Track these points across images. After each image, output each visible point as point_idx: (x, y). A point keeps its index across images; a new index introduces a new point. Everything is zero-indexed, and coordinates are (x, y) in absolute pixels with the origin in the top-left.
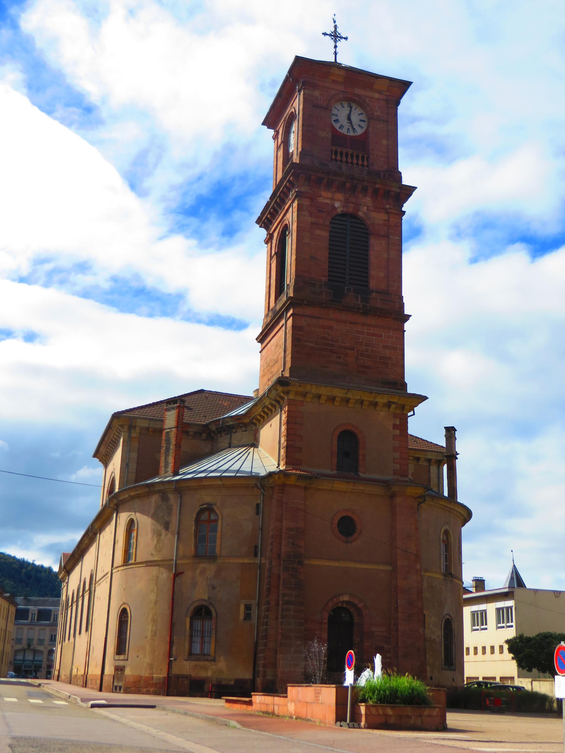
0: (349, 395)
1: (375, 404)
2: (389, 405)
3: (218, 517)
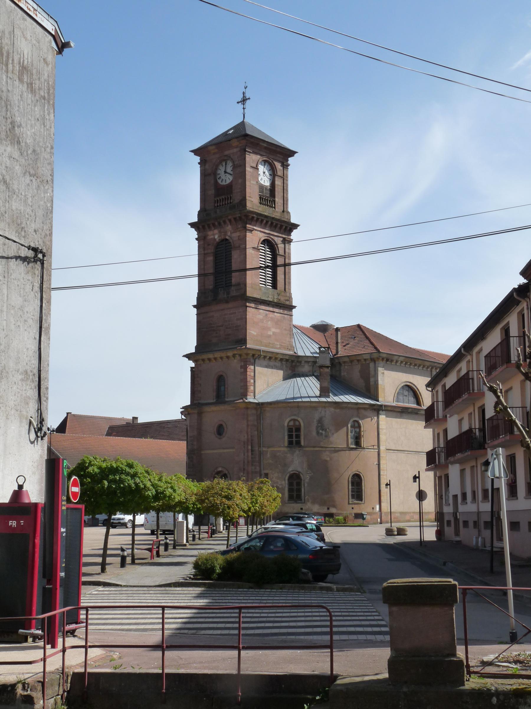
0: (216, 356)
1: (228, 357)
2: (234, 356)
3: (299, 422)
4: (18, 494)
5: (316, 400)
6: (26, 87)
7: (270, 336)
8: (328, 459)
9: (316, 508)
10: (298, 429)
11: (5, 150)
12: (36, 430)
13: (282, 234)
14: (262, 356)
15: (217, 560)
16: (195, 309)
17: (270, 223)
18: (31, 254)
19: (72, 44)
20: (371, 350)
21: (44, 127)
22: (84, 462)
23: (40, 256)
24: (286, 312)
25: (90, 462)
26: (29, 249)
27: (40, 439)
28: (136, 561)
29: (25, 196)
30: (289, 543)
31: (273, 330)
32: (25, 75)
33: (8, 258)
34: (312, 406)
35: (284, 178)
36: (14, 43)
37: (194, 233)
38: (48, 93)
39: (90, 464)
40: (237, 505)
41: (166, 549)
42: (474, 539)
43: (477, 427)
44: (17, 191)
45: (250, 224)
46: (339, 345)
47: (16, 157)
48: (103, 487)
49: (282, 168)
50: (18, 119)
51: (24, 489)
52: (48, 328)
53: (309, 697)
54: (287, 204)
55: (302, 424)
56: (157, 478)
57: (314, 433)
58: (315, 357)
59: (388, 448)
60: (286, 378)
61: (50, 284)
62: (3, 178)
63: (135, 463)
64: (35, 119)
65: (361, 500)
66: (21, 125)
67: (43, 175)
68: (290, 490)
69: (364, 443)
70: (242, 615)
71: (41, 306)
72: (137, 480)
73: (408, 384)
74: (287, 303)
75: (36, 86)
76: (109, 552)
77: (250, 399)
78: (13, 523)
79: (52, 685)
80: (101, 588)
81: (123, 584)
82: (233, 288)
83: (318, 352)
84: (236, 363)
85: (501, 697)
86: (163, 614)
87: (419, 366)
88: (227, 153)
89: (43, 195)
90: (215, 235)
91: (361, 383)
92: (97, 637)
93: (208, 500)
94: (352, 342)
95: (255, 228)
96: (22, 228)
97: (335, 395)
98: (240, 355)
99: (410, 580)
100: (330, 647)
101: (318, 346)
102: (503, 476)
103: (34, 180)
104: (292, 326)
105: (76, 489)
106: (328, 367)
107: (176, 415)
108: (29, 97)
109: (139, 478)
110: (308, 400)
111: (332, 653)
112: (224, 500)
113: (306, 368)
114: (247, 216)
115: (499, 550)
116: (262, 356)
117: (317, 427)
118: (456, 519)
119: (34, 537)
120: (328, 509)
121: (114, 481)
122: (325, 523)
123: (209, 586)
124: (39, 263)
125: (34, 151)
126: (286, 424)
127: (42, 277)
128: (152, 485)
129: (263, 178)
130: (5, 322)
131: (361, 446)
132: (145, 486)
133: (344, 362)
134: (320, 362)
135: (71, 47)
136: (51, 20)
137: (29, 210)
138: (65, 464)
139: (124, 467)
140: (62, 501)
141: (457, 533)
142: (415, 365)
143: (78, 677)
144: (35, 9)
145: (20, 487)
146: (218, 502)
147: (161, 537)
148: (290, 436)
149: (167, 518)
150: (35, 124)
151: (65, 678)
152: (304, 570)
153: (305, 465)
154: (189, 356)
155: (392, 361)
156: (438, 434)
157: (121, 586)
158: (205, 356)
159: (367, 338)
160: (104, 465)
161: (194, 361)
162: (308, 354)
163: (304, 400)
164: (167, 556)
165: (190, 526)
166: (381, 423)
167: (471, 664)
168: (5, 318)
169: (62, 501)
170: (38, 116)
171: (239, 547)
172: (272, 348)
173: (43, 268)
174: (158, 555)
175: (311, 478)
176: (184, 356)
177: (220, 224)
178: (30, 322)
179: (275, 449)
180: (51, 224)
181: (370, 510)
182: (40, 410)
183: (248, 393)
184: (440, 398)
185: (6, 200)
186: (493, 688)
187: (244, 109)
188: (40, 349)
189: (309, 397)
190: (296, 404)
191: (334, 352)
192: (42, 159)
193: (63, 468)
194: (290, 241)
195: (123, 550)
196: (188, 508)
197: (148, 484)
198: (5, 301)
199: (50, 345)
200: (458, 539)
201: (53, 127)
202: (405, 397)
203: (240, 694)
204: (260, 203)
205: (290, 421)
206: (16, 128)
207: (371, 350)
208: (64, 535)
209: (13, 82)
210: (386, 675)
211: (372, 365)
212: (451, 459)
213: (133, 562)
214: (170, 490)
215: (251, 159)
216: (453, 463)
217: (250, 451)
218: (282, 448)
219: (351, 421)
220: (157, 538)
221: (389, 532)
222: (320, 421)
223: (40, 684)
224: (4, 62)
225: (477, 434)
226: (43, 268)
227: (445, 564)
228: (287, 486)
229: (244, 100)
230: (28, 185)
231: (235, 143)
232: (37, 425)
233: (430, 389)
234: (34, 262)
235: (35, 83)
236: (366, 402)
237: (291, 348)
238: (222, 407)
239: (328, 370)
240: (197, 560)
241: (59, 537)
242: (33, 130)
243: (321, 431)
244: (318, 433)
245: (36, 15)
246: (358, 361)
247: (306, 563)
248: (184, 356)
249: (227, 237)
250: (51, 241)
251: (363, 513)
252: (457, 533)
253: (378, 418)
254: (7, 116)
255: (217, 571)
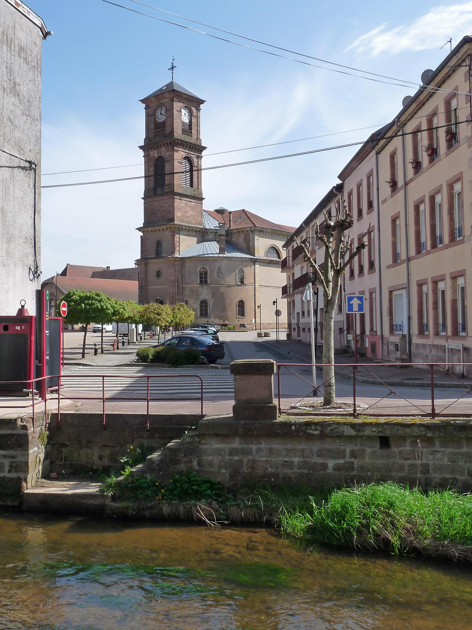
0: (156, 229)
1: (163, 230)
2: (167, 229)
4: (21, 311)
5: (217, 255)
6: (23, 60)
7: (189, 217)
8: (224, 291)
9: (216, 321)
10: (206, 273)
11: (10, 100)
12: (34, 273)
13: (196, 153)
14: (184, 229)
15: (150, 351)
16: (143, 200)
17: (188, 146)
18: (27, 165)
19: (52, 33)
20: (250, 225)
21: (35, 85)
22: (70, 293)
23: (33, 166)
24: (198, 202)
25: (74, 293)
26: (26, 162)
27: (36, 278)
28: (104, 352)
29: (23, 128)
30: (194, 341)
31: (191, 213)
32: (22, 53)
33: (13, 167)
34: (214, 260)
35: (198, 118)
36: (15, 33)
37: (142, 153)
38: (37, 64)
39: (74, 294)
40: (164, 319)
41: (123, 345)
42: (308, 339)
43: (311, 272)
44: (18, 125)
45: (176, 147)
46: (231, 222)
47: (17, 104)
48: (82, 308)
49: (196, 111)
50: (18, 80)
51: (25, 308)
52: (40, 211)
53: (189, 427)
54: (199, 134)
55: (208, 271)
56: (114, 303)
57: (216, 276)
58: (217, 229)
59: (260, 285)
60: (198, 243)
61: (40, 184)
62: (9, 118)
63: (101, 293)
64: (29, 80)
65: (244, 316)
66: (20, 84)
67: (34, 115)
68: (201, 310)
69: (246, 282)
70: (149, 380)
71: (35, 197)
72: (102, 304)
73: (273, 246)
74: (199, 196)
75: (29, 59)
76: (86, 347)
77: (177, 255)
78: (18, 328)
79: (39, 420)
80: (81, 367)
81: (94, 365)
82: (166, 187)
83: (218, 226)
84: (168, 234)
85: (297, 426)
86: (103, 379)
87: (280, 234)
88: (162, 102)
89: (34, 128)
90: (155, 154)
91: (244, 245)
92: (73, 394)
93: (147, 315)
94: (239, 220)
95: (179, 149)
96: (22, 149)
97: (229, 253)
98: (170, 228)
99: (247, 360)
100: (201, 399)
101: (218, 223)
102: (312, 300)
103: (29, 119)
104: (202, 211)
105: (65, 309)
106: (224, 235)
107: (133, 266)
108: (24, 66)
109: (103, 302)
110: (212, 255)
111: (202, 403)
112: (156, 315)
113: (211, 236)
114: (174, 142)
115: (321, 345)
116: (184, 229)
117: (218, 272)
118: (299, 327)
119: (31, 336)
120: (224, 321)
121: (88, 304)
122: (222, 329)
123: (145, 366)
124: (32, 170)
125: (28, 100)
126: (198, 270)
127: (35, 179)
128: (111, 307)
129: (184, 117)
130: (12, 207)
131: (244, 284)
132: (107, 307)
133: (234, 233)
134: (219, 233)
135: (51, 34)
136: (38, 18)
137: (26, 137)
138: (47, 293)
139: (94, 296)
140: (46, 315)
141: (299, 336)
142: (278, 234)
143: (54, 416)
144: (28, 12)
145: (23, 307)
146: (152, 317)
147: (121, 338)
148: (201, 278)
149: (123, 327)
150: (29, 83)
151: (47, 416)
152: (202, 357)
153: (210, 295)
154: (139, 229)
155: (263, 232)
156: (289, 276)
157: (93, 366)
158: (149, 229)
159: (248, 218)
160: (82, 295)
161: (143, 232)
162: (213, 228)
163: (209, 255)
164: (123, 349)
165: (140, 331)
166: (256, 269)
167: (281, 408)
168: (12, 205)
169: (46, 315)
170: (31, 78)
171: (164, 343)
172: (190, 224)
173: (35, 173)
174: (118, 348)
175: (214, 303)
176: (136, 229)
177: (157, 147)
178: (28, 207)
179: (192, 285)
180: (40, 146)
181: (249, 322)
182: (35, 261)
183: (176, 252)
184: (291, 255)
185: (11, 131)
186: (293, 421)
187: (172, 73)
188: (34, 223)
189: (213, 254)
190: (205, 258)
191: (228, 226)
192: (33, 105)
193: (46, 295)
194: (201, 157)
195: (95, 345)
196: (135, 320)
197: (109, 306)
198: (12, 194)
199: (41, 221)
200: (299, 338)
201: (40, 85)
202: (271, 254)
203: (149, 425)
204: (183, 134)
205: (201, 268)
206: (17, 86)
207: (250, 225)
208: (48, 334)
209: (14, 57)
210: (232, 415)
211: (251, 234)
212: (296, 291)
213: (102, 352)
214: (122, 309)
215: (177, 105)
216: (297, 293)
217: (177, 287)
218: (196, 284)
219: (238, 268)
220: (117, 338)
221: (259, 335)
222: (219, 268)
223: (31, 419)
224: (9, 45)
225: (311, 276)
226: (35, 173)
227: (289, 353)
228: (199, 307)
229: (172, 68)
230: (25, 122)
231: (167, 95)
232: (34, 270)
233: (285, 249)
234: (29, 170)
235: (29, 58)
236: (247, 257)
237: (202, 223)
238: (159, 260)
239: (224, 237)
240: (138, 351)
241: (45, 336)
242: (28, 87)
243: (220, 275)
244: (218, 275)
245: (29, 15)
246: (243, 232)
247: (203, 353)
248: (136, 229)
249: (162, 155)
250: (40, 156)
251: (245, 324)
252: (299, 336)
253: (255, 267)
254: (11, 79)
255: (150, 357)
